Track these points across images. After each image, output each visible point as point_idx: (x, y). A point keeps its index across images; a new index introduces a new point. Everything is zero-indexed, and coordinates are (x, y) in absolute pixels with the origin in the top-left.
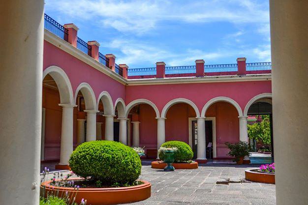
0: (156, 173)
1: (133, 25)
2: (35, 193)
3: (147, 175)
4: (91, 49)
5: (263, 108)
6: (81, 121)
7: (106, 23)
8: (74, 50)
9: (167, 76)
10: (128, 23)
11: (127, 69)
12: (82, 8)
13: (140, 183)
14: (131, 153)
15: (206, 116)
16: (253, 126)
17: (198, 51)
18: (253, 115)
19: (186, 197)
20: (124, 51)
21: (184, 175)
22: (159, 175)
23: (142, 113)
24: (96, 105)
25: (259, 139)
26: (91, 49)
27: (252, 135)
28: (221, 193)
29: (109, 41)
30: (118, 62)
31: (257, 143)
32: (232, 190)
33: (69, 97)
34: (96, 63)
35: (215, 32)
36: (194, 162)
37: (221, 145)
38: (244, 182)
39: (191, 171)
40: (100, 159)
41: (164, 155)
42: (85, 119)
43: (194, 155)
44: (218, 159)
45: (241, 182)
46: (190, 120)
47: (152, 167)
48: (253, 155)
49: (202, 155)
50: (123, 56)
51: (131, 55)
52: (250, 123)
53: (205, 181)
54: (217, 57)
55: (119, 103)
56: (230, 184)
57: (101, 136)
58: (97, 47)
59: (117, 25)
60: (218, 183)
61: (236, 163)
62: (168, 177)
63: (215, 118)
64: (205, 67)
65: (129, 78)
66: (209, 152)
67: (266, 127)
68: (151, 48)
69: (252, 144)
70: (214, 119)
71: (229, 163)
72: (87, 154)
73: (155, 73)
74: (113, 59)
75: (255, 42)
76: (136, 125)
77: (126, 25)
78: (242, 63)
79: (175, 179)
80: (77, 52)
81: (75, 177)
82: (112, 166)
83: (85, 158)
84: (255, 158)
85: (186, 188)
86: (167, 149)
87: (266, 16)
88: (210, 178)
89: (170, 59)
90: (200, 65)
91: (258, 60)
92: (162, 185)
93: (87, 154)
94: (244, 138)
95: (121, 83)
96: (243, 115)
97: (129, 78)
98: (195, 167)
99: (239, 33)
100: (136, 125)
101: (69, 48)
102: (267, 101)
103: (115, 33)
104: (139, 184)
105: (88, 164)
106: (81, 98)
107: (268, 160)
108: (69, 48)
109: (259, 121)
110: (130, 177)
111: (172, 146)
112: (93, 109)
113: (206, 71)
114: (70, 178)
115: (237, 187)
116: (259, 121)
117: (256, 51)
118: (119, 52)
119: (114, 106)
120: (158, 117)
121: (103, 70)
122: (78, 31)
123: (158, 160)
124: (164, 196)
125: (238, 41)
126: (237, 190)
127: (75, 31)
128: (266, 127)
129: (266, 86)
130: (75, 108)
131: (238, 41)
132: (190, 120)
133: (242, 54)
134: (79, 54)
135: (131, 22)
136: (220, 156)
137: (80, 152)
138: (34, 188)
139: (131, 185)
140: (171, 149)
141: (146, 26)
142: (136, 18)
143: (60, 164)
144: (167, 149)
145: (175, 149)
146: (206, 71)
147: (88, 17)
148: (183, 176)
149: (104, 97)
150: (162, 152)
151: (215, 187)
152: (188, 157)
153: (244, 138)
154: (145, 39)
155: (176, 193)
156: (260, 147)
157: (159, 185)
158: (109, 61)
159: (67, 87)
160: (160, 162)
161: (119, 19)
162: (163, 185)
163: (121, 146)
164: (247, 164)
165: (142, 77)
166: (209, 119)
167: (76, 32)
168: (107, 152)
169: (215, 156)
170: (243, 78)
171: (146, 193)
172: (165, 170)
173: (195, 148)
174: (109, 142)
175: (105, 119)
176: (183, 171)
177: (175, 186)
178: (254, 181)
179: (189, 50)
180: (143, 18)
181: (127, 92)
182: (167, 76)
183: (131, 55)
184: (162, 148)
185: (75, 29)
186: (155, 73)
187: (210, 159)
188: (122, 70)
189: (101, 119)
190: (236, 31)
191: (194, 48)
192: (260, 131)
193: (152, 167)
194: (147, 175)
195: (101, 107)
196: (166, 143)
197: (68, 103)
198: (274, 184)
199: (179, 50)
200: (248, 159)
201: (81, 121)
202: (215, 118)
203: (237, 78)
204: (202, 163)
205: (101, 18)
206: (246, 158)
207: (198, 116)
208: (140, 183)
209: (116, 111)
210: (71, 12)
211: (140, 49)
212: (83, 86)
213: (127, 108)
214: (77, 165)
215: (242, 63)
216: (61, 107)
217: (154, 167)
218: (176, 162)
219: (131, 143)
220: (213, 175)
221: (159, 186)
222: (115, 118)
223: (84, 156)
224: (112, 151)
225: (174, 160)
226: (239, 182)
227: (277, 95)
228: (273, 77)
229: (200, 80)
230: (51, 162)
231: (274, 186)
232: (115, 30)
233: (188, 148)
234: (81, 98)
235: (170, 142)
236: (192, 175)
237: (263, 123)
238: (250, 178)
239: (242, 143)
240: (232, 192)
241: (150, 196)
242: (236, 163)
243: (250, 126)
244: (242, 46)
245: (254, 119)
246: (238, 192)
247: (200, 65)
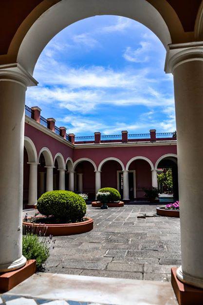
0: (95, 210)
1: (79, 107)
2: (19, 234)
3: (91, 213)
4: (50, 124)
5: (170, 164)
6: (42, 174)
7: (62, 105)
8: (42, 126)
9: (102, 142)
10: (76, 106)
11: (74, 137)
12: (45, 96)
13: (86, 219)
14: (80, 199)
15: (129, 169)
16: (161, 175)
17: (123, 124)
18: (162, 168)
19: (117, 229)
20: (73, 124)
21: (114, 211)
22: (98, 212)
23: (85, 170)
24: (53, 163)
25: (164, 183)
26: (50, 124)
27: (160, 181)
28: (141, 225)
29: (62, 117)
30: (68, 132)
31: (164, 187)
32: (148, 222)
33: (34, 157)
34: (54, 133)
35: (133, 113)
36: (121, 202)
37: (139, 190)
38: (156, 216)
39: (119, 209)
40: (58, 203)
41: (100, 197)
42: (44, 172)
43: (121, 197)
44: (137, 199)
45: (154, 216)
46: (118, 172)
47: (92, 206)
48: (161, 195)
49: (126, 196)
50: (72, 127)
51: (77, 127)
52: (159, 173)
53: (129, 216)
54: (137, 128)
55: (69, 161)
56: (146, 218)
57: (56, 187)
58: (54, 123)
59: (68, 107)
60: (138, 217)
61: (149, 202)
62: (104, 214)
63: (135, 171)
64: (128, 136)
65: (76, 143)
66: (131, 193)
67: (169, 176)
68: (92, 122)
69: (160, 189)
70: (134, 172)
71: (145, 202)
72: (49, 200)
73: (94, 140)
74: (65, 130)
75: (163, 118)
76: (81, 176)
77: (75, 107)
78: (153, 133)
79: (108, 215)
80: (39, 126)
81: (40, 216)
82: (67, 208)
83: (48, 203)
84: (162, 198)
85: (116, 222)
86: (102, 193)
87: (172, 101)
88: (133, 214)
89: (104, 129)
90: (125, 134)
91: (163, 130)
92: (100, 220)
93: (49, 200)
94: (155, 184)
95: (67, 145)
96: (154, 169)
97: (76, 143)
98: (122, 205)
99: (151, 113)
100: (81, 176)
101: (35, 123)
102: (174, 161)
103: (67, 112)
104: (85, 220)
105: (50, 208)
106: (42, 158)
107: (171, 200)
108: (35, 123)
109: (164, 172)
110: (78, 214)
111: (106, 191)
112: (51, 166)
113: (129, 138)
114: (37, 216)
115: (151, 220)
116: (164, 172)
117: (162, 124)
118: (69, 125)
119: (53, 159)
120: (96, 170)
121: (52, 135)
122: (41, 112)
123: (97, 201)
124: (102, 229)
125: (150, 117)
126: (151, 222)
127: (39, 112)
128: (169, 176)
129: (173, 149)
130: (54, 168)
131: (150, 117)
132: (118, 172)
133: (153, 126)
134: (40, 127)
135: (79, 105)
136: (139, 197)
137: (45, 199)
138: (19, 230)
139: (80, 221)
140: (105, 193)
141: (89, 107)
142: (82, 102)
143: (29, 204)
144: (102, 193)
145: (109, 193)
146: (129, 138)
147: (50, 102)
148: (115, 213)
149: (58, 157)
150: (99, 195)
151: (136, 221)
152: (117, 199)
153: (155, 184)
154: (88, 116)
155: (110, 226)
156: (164, 189)
157: (98, 220)
158: (62, 132)
159: (33, 151)
160: (98, 202)
161: (70, 103)
162: (101, 220)
163: (71, 194)
164: (157, 203)
165: (85, 142)
166: (131, 171)
167: (39, 112)
168: (63, 199)
169: (135, 197)
170: (154, 143)
171: (89, 227)
172: (102, 208)
173: (121, 192)
174: (62, 191)
175: (29, 167)
176: (113, 209)
177: (109, 220)
178: (162, 216)
179: (118, 124)
180: (86, 102)
181: (74, 153)
182: (102, 142)
183: (77, 127)
184: (99, 193)
185: (39, 110)
186: (94, 140)
187: (132, 201)
188: (71, 138)
189: (56, 173)
190: (149, 111)
191: (121, 122)
192: (166, 179)
193: (92, 206)
194: (91, 213)
195: (56, 163)
196: (102, 189)
197: (34, 162)
198: (179, 217)
199: (110, 123)
200: (158, 199)
201: (42, 174)
202: (135, 171)
203: (150, 144)
204: (127, 202)
205: (58, 102)
206: (157, 199)
207: (123, 169)
208: (86, 219)
209: (67, 168)
210: (38, 98)
211: (84, 122)
212: (44, 150)
213: (74, 164)
214: (42, 208)
215: (153, 133)
216: (59, 171)
217: (94, 205)
218: (108, 202)
219: (77, 191)
220: (135, 211)
221: (98, 221)
222: (66, 171)
223: (47, 201)
224: (67, 198)
225: (107, 201)
226: (153, 217)
227: (180, 155)
228: (177, 142)
229: (125, 145)
230: (27, 206)
231: (179, 219)
232: (67, 110)
233: (116, 192)
234: (42, 158)
235: (104, 189)
236: (120, 211)
237: (167, 173)
238: (160, 213)
239: (154, 188)
240: (148, 224)
241: (92, 228)
242: (149, 202)
243: (158, 175)
244: (153, 121)
245: (162, 170)
246: (153, 224)
247: (125, 134)
